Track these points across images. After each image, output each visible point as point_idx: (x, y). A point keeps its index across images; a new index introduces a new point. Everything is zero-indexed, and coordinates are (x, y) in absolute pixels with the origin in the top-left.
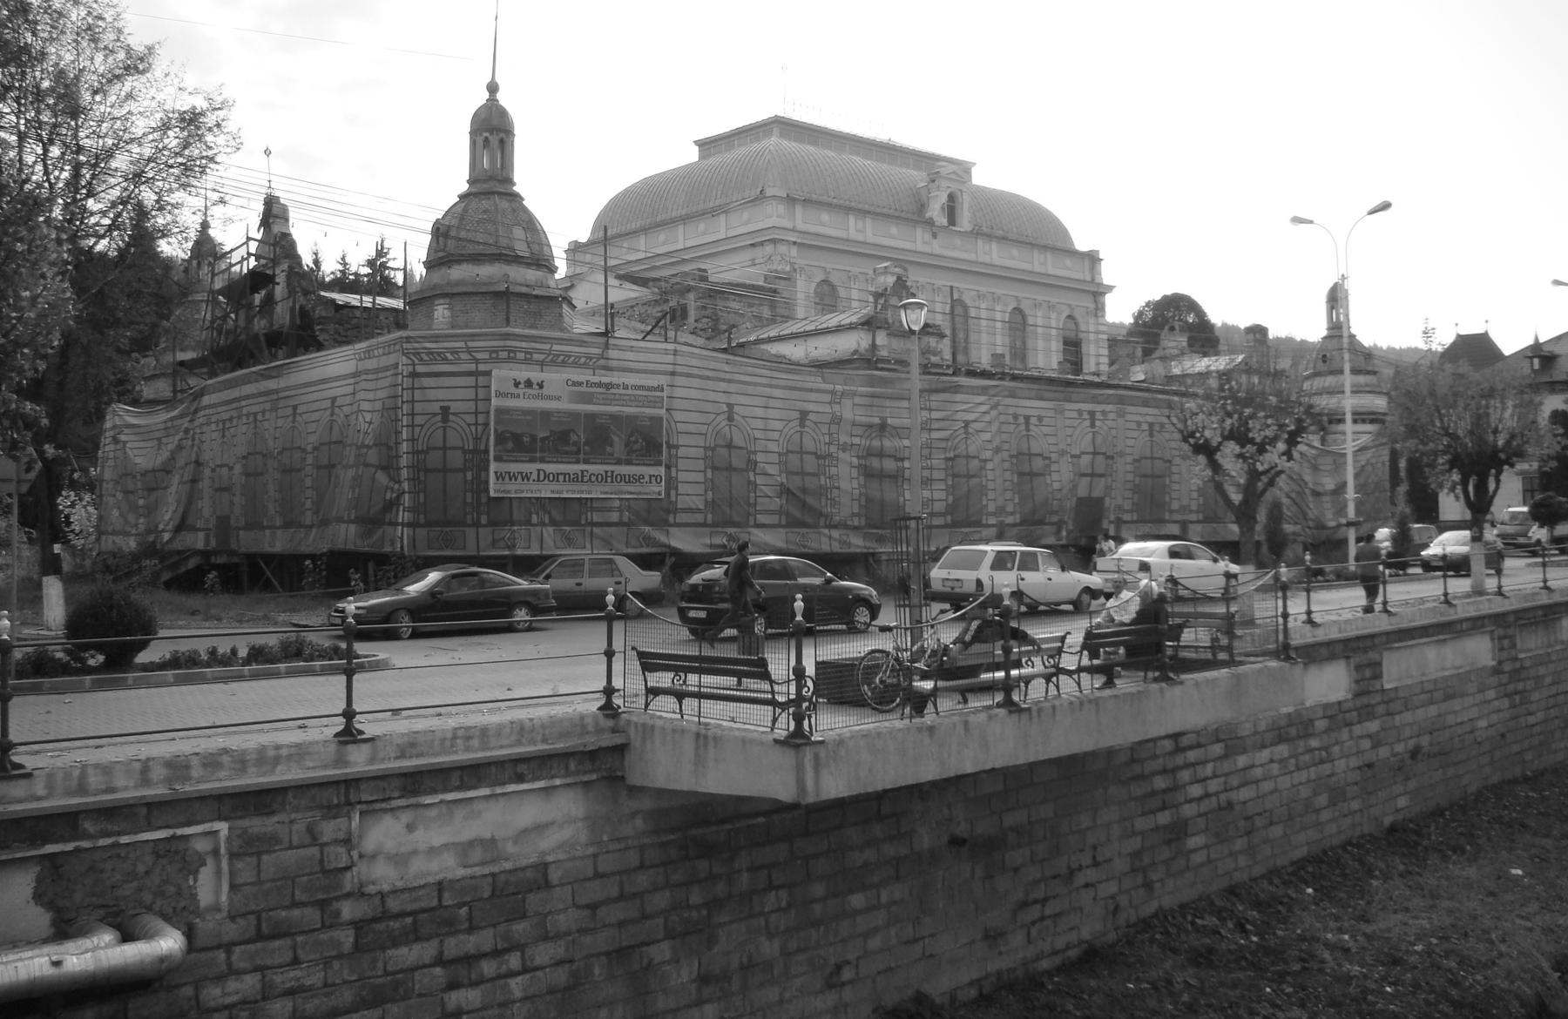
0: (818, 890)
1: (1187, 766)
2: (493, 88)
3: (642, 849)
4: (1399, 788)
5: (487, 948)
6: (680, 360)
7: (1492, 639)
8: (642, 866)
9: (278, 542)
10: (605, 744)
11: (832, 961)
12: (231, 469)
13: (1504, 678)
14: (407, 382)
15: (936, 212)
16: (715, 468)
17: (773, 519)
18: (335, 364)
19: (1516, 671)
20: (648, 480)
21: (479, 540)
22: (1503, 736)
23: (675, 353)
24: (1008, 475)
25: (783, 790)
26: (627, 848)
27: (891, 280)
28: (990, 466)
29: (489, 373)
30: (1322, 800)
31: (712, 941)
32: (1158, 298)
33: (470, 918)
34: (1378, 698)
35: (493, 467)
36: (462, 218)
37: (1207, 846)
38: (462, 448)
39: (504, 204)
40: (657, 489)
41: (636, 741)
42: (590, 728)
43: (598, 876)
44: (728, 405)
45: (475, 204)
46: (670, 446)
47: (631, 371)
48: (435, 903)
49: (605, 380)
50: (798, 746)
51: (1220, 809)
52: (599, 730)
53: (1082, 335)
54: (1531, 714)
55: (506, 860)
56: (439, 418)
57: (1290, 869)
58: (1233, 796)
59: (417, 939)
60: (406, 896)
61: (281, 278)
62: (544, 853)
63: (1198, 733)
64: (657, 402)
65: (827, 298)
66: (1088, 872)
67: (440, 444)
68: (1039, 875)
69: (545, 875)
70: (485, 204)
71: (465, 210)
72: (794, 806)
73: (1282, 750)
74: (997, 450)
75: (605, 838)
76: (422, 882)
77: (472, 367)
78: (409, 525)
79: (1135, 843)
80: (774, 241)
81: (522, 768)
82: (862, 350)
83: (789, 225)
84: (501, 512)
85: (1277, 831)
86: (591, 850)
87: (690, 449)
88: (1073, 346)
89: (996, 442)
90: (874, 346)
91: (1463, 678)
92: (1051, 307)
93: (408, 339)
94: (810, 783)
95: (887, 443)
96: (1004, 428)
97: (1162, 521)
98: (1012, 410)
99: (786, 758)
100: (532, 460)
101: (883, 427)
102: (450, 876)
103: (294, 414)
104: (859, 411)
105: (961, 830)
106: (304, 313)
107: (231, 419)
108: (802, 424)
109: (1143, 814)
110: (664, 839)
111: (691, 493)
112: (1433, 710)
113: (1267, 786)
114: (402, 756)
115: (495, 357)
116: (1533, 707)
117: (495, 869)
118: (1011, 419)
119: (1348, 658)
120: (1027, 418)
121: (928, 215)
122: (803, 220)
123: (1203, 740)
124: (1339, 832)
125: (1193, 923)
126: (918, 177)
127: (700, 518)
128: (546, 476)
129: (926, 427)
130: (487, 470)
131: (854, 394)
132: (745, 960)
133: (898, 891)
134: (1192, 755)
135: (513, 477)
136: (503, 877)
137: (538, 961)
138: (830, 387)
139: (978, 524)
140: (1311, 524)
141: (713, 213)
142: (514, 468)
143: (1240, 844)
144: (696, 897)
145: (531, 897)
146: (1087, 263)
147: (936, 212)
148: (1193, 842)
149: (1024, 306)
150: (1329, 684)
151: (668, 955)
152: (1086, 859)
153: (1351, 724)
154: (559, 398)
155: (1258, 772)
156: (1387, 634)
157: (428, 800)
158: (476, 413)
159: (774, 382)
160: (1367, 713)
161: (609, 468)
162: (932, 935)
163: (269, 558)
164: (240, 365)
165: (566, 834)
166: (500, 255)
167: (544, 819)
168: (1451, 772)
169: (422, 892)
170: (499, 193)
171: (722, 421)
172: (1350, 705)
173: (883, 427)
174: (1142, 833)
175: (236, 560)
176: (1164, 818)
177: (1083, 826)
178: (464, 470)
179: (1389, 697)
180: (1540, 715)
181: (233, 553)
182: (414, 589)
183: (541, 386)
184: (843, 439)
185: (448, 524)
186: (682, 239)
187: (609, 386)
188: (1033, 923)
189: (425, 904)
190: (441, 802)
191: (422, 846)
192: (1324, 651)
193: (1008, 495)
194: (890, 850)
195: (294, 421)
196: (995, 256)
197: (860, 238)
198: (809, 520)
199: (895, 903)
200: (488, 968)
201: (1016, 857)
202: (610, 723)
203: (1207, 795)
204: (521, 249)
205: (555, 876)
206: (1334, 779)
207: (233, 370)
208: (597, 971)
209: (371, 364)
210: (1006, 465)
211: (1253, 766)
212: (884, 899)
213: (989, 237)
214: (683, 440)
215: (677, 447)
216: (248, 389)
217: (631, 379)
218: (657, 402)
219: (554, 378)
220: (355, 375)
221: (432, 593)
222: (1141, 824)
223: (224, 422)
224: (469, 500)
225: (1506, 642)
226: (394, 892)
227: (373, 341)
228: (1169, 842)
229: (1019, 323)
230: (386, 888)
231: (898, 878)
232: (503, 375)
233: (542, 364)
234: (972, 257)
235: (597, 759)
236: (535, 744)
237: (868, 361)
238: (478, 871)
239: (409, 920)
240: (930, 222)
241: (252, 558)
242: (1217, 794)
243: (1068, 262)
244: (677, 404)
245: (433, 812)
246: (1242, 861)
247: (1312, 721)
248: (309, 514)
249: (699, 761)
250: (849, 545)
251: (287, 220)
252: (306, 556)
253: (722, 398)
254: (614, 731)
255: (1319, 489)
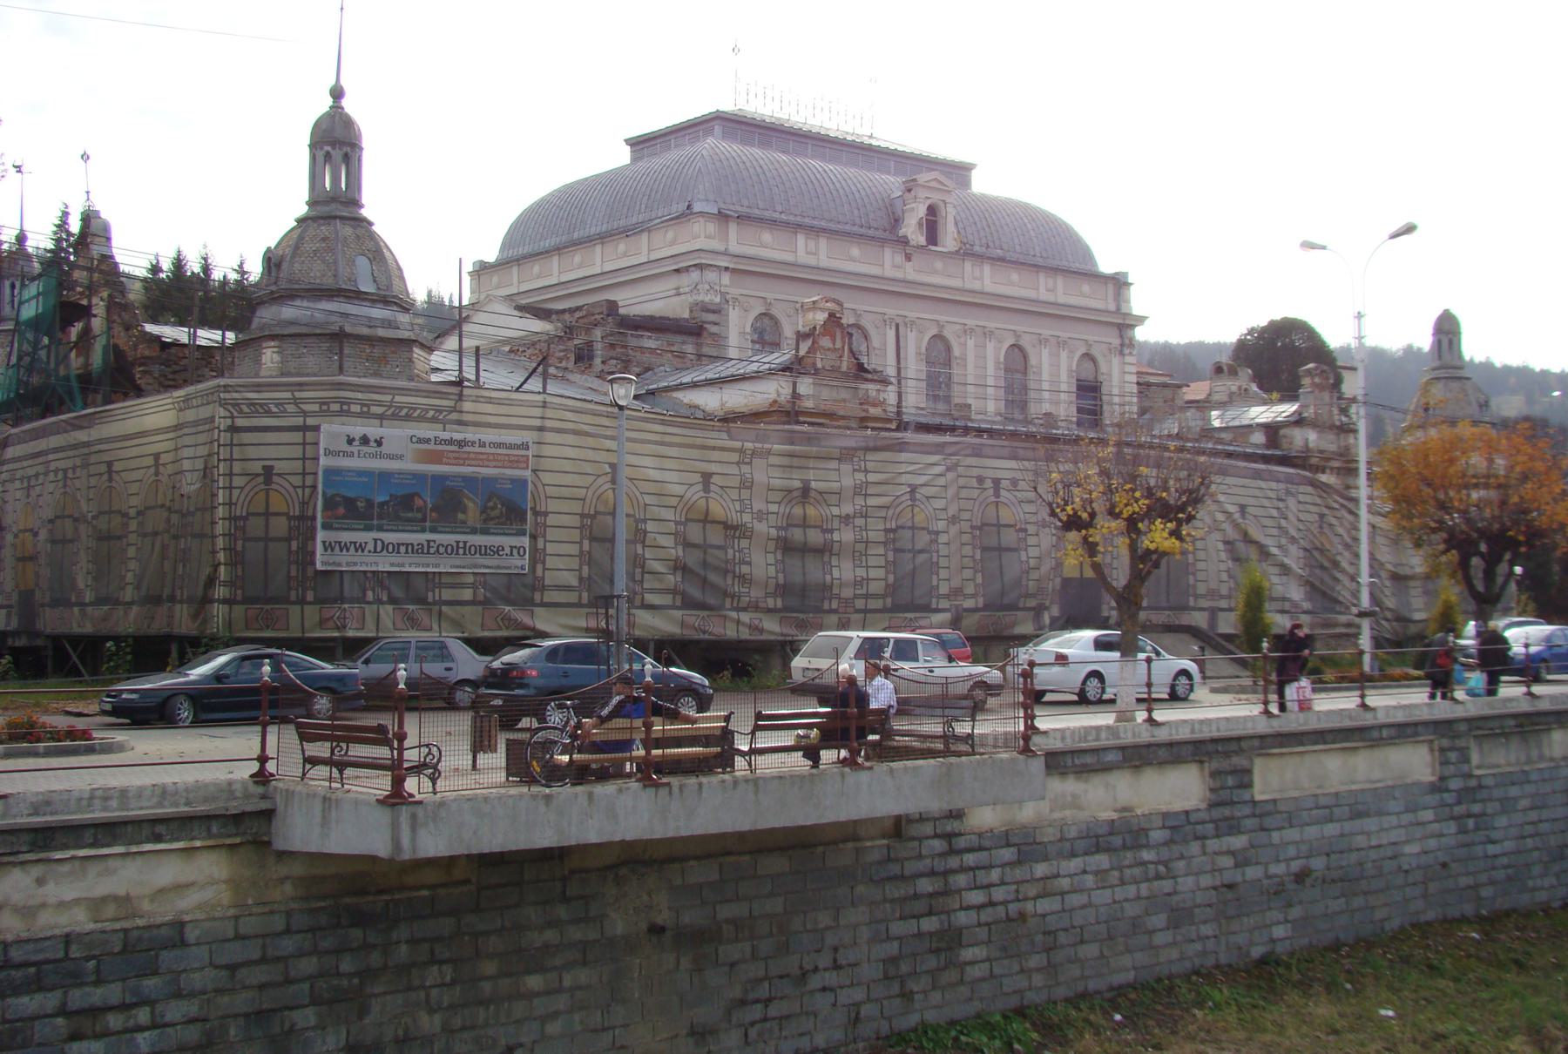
0: (490, 968)
1: (963, 869)
2: (337, 93)
3: (289, 914)
4: (1275, 915)
5: (114, 1000)
6: (549, 413)
7: (1432, 750)
8: (288, 931)
9: (79, 623)
10: (249, 808)
11: (503, 1042)
12: (36, 534)
13: (1449, 798)
14: (225, 438)
15: (911, 228)
16: (593, 539)
17: (665, 600)
18: (154, 414)
19: (1467, 789)
20: (508, 552)
21: (305, 620)
22: (1444, 865)
23: (544, 405)
24: (967, 550)
25: (379, 846)
26: (272, 912)
27: (821, 317)
28: (943, 538)
29: (317, 429)
30: (1159, 920)
31: (363, 1011)
32: (1263, 323)
33: (98, 971)
34: (1247, 810)
35: (321, 535)
36: (297, 247)
37: (988, 960)
38: (287, 514)
39: (347, 231)
40: (519, 563)
41: (281, 808)
42: (238, 794)
43: (239, 937)
44: (613, 466)
45: (312, 230)
46: (536, 513)
47: (490, 425)
48: (61, 954)
49: (457, 436)
50: (394, 805)
51: (1009, 919)
52: (247, 796)
53: (1101, 378)
54: (1493, 842)
55: (141, 917)
56: (261, 479)
57: (1108, 995)
58: (1029, 907)
59: (41, 989)
60: (31, 947)
61: (99, 308)
62: (182, 912)
63: (980, 835)
64: (522, 462)
65: (765, 335)
66: (827, 975)
67: (262, 510)
68: (761, 973)
69: (182, 934)
70: (325, 230)
71: (301, 238)
72: (391, 861)
73: (1102, 860)
74: (954, 520)
75: (250, 902)
76: (49, 933)
77: (299, 421)
78: (225, 601)
79: (893, 948)
80: (700, 267)
81: (160, 829)
82: (782, 399)
83: (720, 247)
84: (330, 589)
85: (1090, 951)
86: (232, 912)
87: (562, 519)
88: (1089, 390)
89: (952, 511)
90: (795, 395)
91: (1388, 792)
92: (1061, 344)
93: (226, 388)
94: (406, 841)
95: (811, 511)
96: (964, 493)
97: (1185, 608)
98: (975, 472)
99: (383, 816)
100: (368, 528)
101: (806, 491)
102: (78, 929)
103: (110, 472)
104: (777, 473)
105: (664, 917)
106: (118, 353)
107: (37, 475)
108: (706, 489)
109: (901, 918)
110: (315, 904)
111: (562, 566)
112: (1331, 829)
113: (1075, 900)
114: (36, 813)
115: (325, 410)
116: (1495, 835)
117: (127, 924)
118: (974, 483)
119: (1201, 762)
120: (997, 482)
121: (901, 233)
122: (738, 241)
123: (987, 844)
124: (1181, 959)
125: (956, 1039)
126: (892, 183)
127: (572, 597)
128: (385, 547)
129: (860, 490)
130: (314, 539)
131: (769, 452)
132: (401, 1033)
133: (583, 976)
134: (970, 859)
135: (344, 547)
136: (135, 933)
137: (168, 1018)
138: (738, 444)
139: (927, 609)
140: (1389, 615)
141: (628, 232)
142: (346, 537)
143: (1035, 961)
144: (346, 965)
145: (164, 954)
146: (1111, 288)
147: (911, 228)
148: (968, 954)
149: (1025, 342)
150: (1182, 789)
151: (313, 1021)
152: (824, 960)
153: (1205, 838)
154: (401, 457)
155: (1065, 883)
156: (1262, 737)
157: (59, 855)
158: (304, 474)
159: (667, 439)
160: (1231, 827)
161: (462, 538)
162: (625, 1026)
163: (76, 640)
164: (48, 411)
165: (208, 894)
166: (340, 290)
167: (183, 879)
168: (1358, 902)
169: (48, 943)
170: (342, 218)
171: (604, 484)
172: (1203, 816)
173: (806, 491)
174: (899, 938)
175: (39, 642)
176: (930, 924)
177: (821, 926)
178: (288, 539)
179: (1264, 813)
180: (1509, 845)
181: (37, 634)
182: (199, 671)
183: (379, 443)
184: (758, 505)
185: (269, 601)
186: (600, 261)
187: (462, 443)
188: (753, 1024)
189: (49, 955)
190: (73, 858)
191: (52, 900)
192: (1162, 753)
193: (968, 574)
194: (575, 933)
195: (110, 480)
196: (987, 282)
197: (811, 261)
198: (711, 601)
199: (580, 988)
200: (114, 1021)
201: (731, 952)
202: (260, 790)
203: (992, 904)
204: (367, 287)
205: (191, 935)
206: (1175, 899)
207: (44, 417)
208: (232, 1032)
209: (190, 415)
210: (966, 538)
211: (1058, 876)
212: (567, 982)
213: (980, 258)
214: (553, 506)
215: (546, 514)
216: (55, 441)
217: (490, 436)
218: (522, 462)
219: (396, 435)
220: (177, 427)
221: (218, 676)
222: (898, 928)
223: (29, 478)
224: (293, 573)
225: (1453, 756)
226: (20, 942)
227: (191, 389)
228: (937, 951)
229: (1017, 362)
230: (10, 937)
231: (585, 963)
232: (332, 431)
233: (381, 417)
234: (956, 283)
235: (244, 825)
236: (177, 805)
237: (789, 413)
238: (108, 926)
239: (32, 970)
240: (904, 242)
241: (56, 640)
242: (1005, 903)
243: (1086, 288)
244: (546, 464)
245: (66, 868)
246: (1038, 980)
247: (1145, 831)
248: (129, 589)
249: (325, 822)
250: (762, 631)
251: (109, 239)
252: (109, 638)
253: (602, 456)
254: (264, 797)
255: (1401, 571)
